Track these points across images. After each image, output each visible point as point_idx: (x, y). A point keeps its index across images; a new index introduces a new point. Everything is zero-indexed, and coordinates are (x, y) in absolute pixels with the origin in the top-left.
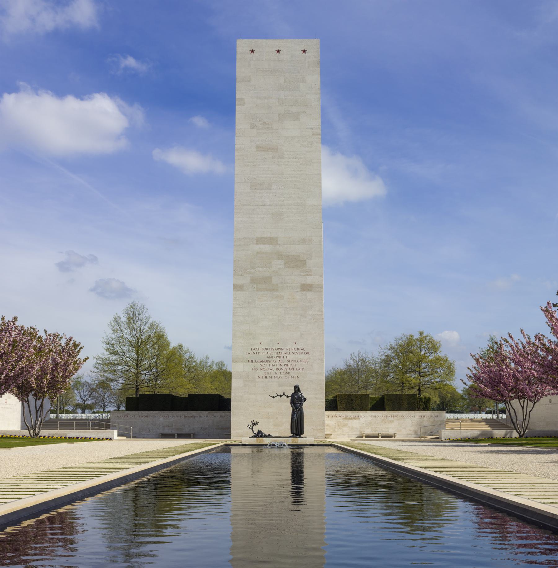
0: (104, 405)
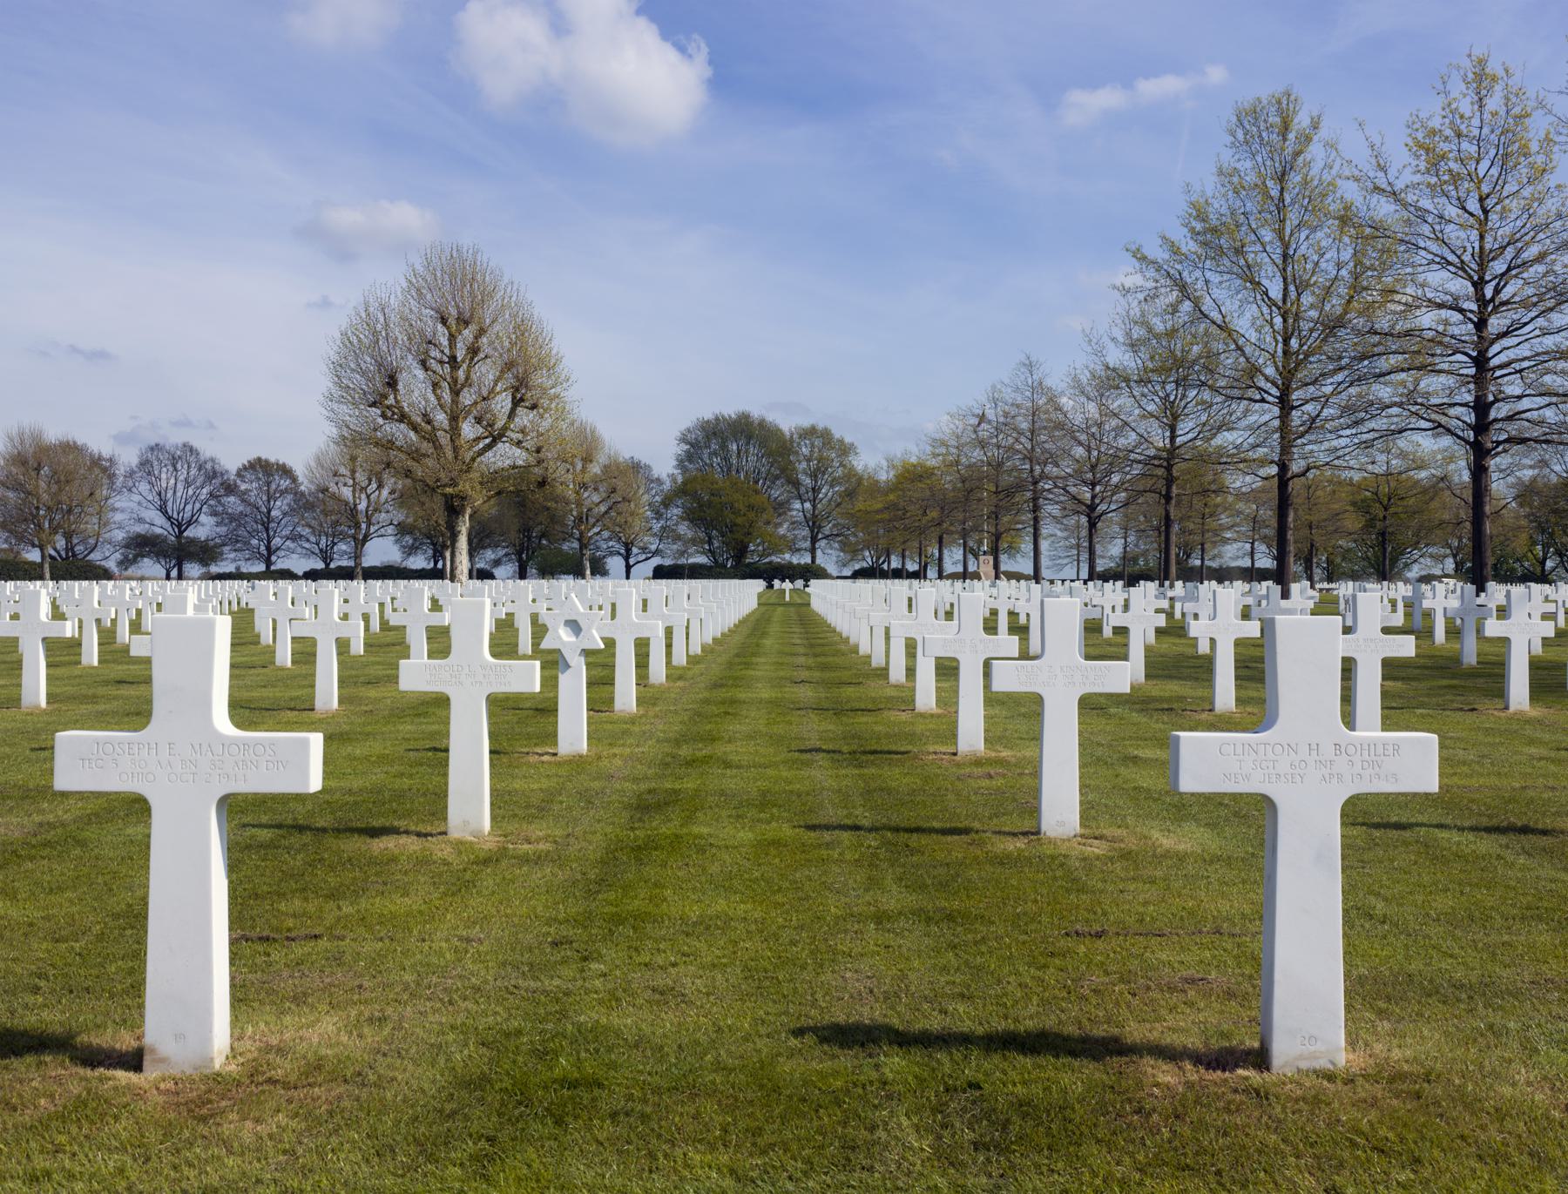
0: (268, 548)
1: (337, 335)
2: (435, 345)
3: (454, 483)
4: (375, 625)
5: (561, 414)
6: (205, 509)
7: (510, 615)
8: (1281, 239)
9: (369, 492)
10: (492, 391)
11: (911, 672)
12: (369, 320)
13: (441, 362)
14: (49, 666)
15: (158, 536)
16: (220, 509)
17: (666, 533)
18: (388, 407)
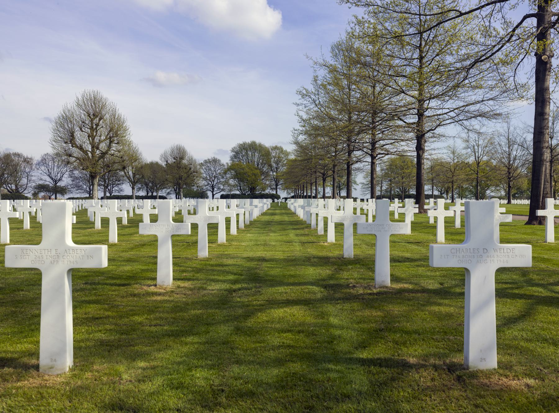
4: (131, 214)
11: (326, 230)
14: (117, 224)
17: (226, 183)
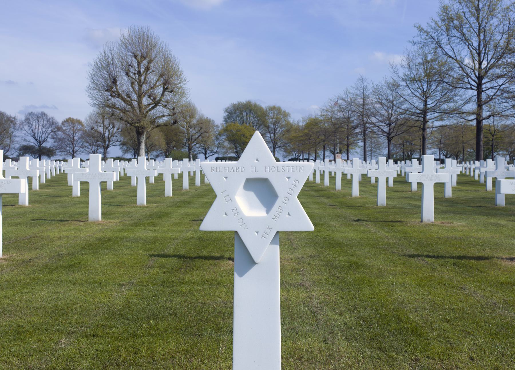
0: (73, 151)
1: (93, 63)
2: (132, 66)
3: (139, 122)
5: (183, 95)
6: (50, 136)
7: (161, 175)
8: (479, 23)
9: (109, 129)
10: (155, 85)
12: (105, 58)
13: (135, 74)
15: (32, 146)
16: (55, 136)
17: (219, 145)
18: (113, 92)
